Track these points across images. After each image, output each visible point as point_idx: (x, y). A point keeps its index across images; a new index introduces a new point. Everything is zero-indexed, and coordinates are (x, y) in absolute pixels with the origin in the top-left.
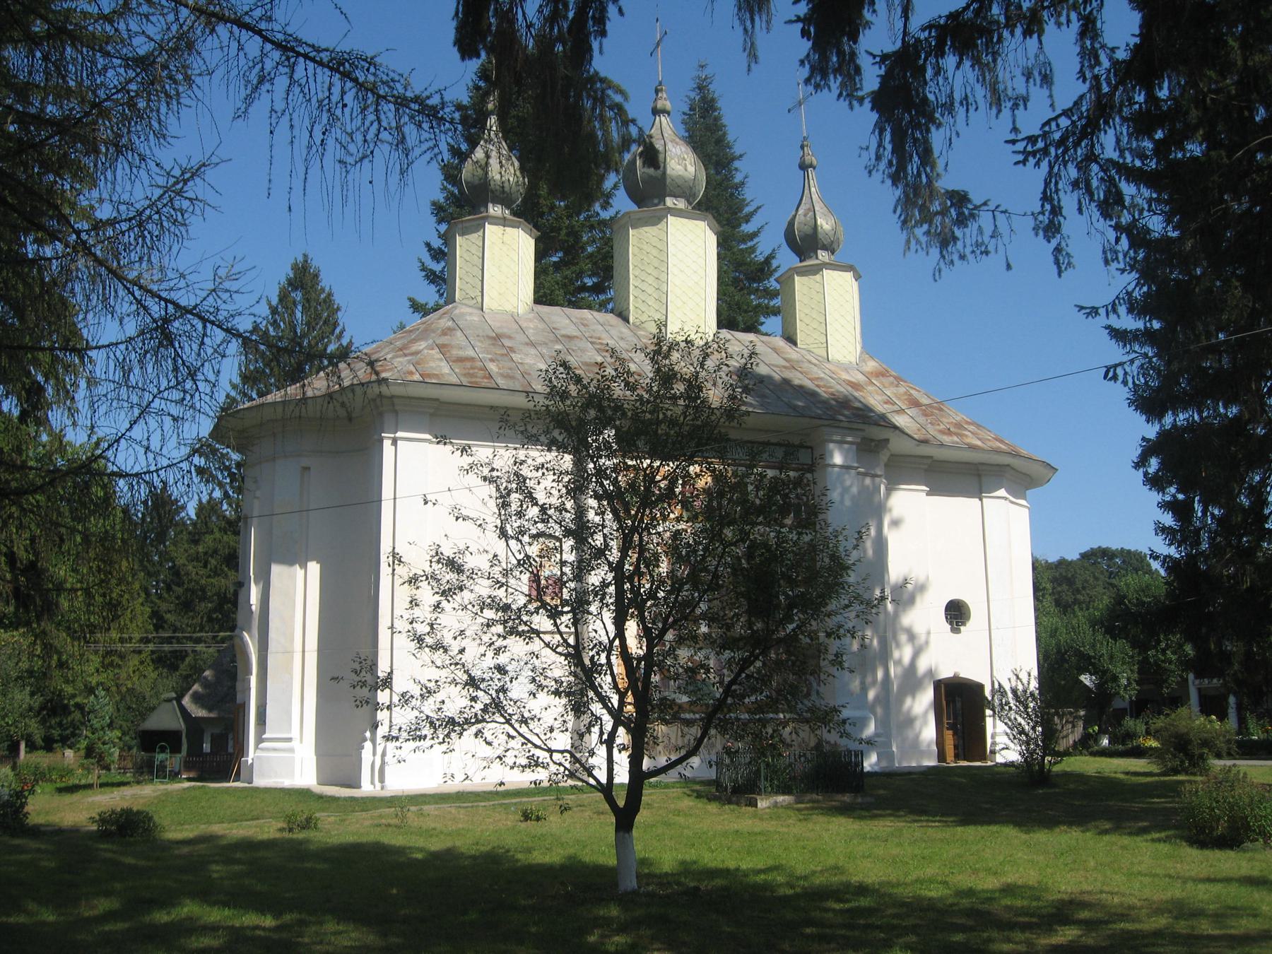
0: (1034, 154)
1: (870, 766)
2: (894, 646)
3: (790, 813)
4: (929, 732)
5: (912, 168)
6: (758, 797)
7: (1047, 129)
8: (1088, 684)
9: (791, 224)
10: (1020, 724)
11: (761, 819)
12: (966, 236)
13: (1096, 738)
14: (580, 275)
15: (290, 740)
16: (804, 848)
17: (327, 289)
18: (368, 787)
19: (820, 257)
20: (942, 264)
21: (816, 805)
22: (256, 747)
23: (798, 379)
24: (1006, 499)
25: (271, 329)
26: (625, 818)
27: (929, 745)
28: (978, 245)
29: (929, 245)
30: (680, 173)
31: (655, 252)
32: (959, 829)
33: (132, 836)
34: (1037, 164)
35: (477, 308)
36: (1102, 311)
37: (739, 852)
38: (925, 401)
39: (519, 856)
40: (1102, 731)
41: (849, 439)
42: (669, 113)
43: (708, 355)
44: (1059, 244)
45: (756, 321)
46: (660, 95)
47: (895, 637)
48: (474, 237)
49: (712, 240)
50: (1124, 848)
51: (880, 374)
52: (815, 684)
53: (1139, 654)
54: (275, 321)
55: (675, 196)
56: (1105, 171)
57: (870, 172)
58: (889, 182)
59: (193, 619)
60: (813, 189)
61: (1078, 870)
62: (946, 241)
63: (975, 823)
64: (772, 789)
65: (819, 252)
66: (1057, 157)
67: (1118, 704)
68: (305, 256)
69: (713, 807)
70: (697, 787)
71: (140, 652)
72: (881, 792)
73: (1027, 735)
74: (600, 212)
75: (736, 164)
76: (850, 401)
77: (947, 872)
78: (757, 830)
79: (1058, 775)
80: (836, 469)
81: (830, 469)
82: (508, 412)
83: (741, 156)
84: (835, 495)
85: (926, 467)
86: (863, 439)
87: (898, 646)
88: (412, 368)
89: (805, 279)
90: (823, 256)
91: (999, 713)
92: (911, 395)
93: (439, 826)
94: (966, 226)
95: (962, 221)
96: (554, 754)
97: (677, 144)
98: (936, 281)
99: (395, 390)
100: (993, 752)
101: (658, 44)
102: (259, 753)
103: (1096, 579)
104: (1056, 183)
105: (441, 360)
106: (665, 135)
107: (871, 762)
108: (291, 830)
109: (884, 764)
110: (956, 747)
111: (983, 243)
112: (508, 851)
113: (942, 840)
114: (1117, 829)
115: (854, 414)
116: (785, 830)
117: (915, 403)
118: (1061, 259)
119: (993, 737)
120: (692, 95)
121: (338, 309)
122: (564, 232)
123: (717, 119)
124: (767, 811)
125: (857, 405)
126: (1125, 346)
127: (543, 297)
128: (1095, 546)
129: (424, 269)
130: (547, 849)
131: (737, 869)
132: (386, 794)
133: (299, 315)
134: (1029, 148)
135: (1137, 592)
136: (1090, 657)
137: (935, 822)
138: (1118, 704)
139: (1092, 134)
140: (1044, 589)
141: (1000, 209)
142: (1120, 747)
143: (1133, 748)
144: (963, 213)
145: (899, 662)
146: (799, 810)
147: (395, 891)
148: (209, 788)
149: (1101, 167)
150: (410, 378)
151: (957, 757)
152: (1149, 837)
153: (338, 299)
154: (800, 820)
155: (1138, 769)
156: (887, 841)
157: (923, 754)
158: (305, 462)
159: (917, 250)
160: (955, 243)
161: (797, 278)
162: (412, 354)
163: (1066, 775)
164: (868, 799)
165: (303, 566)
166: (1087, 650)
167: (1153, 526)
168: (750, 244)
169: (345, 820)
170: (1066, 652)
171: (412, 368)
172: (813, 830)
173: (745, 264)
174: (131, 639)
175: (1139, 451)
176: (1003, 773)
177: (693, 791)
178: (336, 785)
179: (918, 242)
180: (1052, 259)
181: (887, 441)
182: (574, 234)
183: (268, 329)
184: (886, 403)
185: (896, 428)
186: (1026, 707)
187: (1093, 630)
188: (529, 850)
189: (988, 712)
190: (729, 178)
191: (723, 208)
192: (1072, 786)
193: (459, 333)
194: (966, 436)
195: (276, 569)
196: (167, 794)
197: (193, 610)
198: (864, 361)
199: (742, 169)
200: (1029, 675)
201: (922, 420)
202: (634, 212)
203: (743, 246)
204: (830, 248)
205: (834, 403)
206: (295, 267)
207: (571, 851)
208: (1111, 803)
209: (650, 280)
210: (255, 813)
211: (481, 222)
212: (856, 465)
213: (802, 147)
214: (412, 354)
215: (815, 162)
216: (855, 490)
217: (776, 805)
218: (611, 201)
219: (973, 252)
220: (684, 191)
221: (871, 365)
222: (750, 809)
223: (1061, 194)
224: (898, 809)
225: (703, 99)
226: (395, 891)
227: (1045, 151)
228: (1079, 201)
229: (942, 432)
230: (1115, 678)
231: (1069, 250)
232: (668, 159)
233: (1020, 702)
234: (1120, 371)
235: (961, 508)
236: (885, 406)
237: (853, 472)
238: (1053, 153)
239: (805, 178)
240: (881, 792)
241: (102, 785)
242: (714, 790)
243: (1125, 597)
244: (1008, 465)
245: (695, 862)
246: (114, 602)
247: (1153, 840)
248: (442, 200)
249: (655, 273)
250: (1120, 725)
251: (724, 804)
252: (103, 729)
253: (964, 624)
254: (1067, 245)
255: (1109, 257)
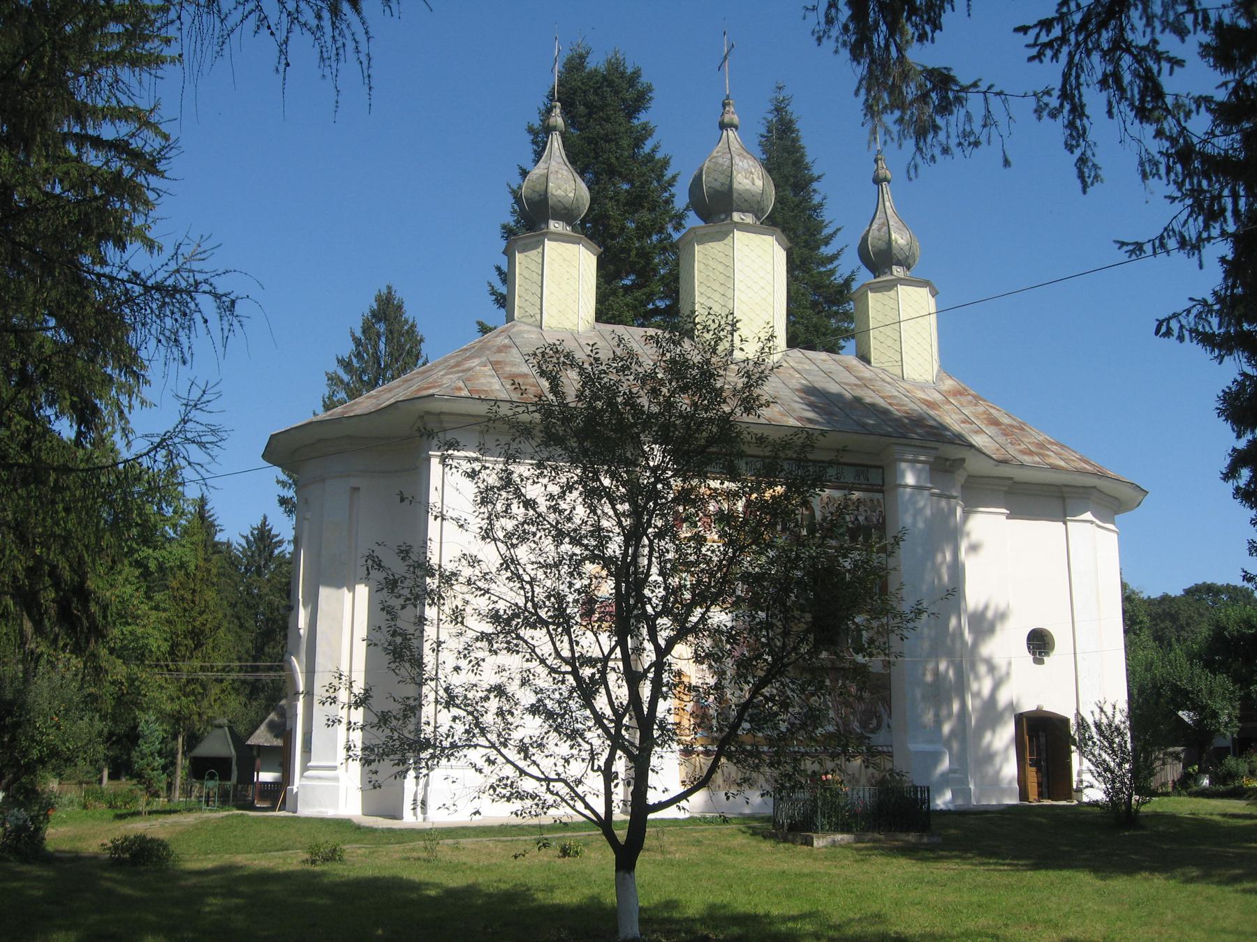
0: (1049, 44)
1: (945, 803)
2: (972, 677)
3: (848, 853)
4: (1010, 769)
5: (879, 39)
6: (814, 835)
7: (1065, 10)
8: (1187, 720)
9: (865, 239)
10: (1104, 761)
11: (815, 859)
12: (951, 125)
13: (1195, 778)
14: (650, 297)
15: (334, 768)
16: (851, 892)
17: (411, 321)
18: (409, 819)
19: (895, 273)
20: (918, 158)
21: (877, 845)
22: (302, 776)
23: (869, 397)
24: (1092, 522)
25: (354, 360)
26: (627, 855)
27: (1010, 782)
28: (966, 135)
29: (902, 135)
30: (747, 187)
31: (721, 268)
32: (1029, 873)
33: (144, 865)
34: (1055, 56)
35: (536, 326)
36: (1148, 248)
37: (777, 896)
38: (1006, 420)
39: (540, 896)
40: (1202, 771)
41: (922, 458)
42: (736, 128)
43: (721, 339)
44: (1083, 154)
45: (835, 345)
46: (727, 109)
47: (973, 666)
48: (534, 254)
49: (781, 256)
50: (1209, 899)
51: (958, 393)
52: (885, 717)
53: (1241, 689)
54: (359, 353)
55: (743, 211)
56: (1139, 62)
57: (819, 39)
58: (845, 54)
59: (274, 648)
60: (887, 204)
61: (1151, 924)
62: (923, 131)
63: (1047, 867)
64: (830, 826)
65: (894, 267)
66: (1078, 44)
67: (1218, 742)
68: (389, 288)
69: (767, 846)
70: (756, 824)
71: (221, 681)
72: (953, 831)
73: (1112, 772)
74: (673, 233)
75: (815, 185)
76: (924, 419)
77: (1000, 923)
78: (806, 871)
79: (1147, 816)
80: (908, 490)
81: (901, 489)
82: (498, 403)
83: (819, 177)
84: (907, 519)
85: (1006, 488)
86: (937, 458)
87: (977, 678)
88: (461, 384)
89: (879, 295)
90: (898, 271)
91: (1082, 745)
92: (991, 414)
93: (469, 860)
94: (951, 113)
95: (945, 108)
96: (552, 784)
97: (744, 157)
98: (910, 179)
99: (446, 407)
100: (1079, 790)
101: (725, 58)
102: (305, 782)
103: (1201, 615)
104: (1078, 77)
105: (493, 376)
106: (733, 149)
107: (943, 800)
108: (313, 862)
109: (960, 802)
110: (1040, 785)
111: (972, 132)
112: (528, 889)
113: (1006, 886)
114: (1205, 877)
115: (927, 432)
116: (836, 871)
117: (995, 422)
118: (1086, 173)
119: (1079, 774)
120: (770, 117)
121: (422, 340)
122: (634, 253)
123: (795, 140)
124: (824, 850)
125: (933, 423)
126: (1213, 350)
127: (602, 315)
128: (1200, 582)
129: (493, 292)
130: (572, 888)
131: (767, 915)
132: (427, 825)
133: (382, 346)
134: (1044, 38)
135: (1238, 624)
136: (1187, 692)
137: (1003, 865)
138: (1218, 742)
139: (1121, 12)
140: (1141, 622)
141: (994, 90)
142: (1222, 788)
143: (1235, 789)
144: (947, 98)
145: (977, 695)
146: (858, 850)
147: (380, 932)
148: (248, 816)
149: (1134, 57)
150: (458, 394)
151: (1041, 795)
152: (1239, 887)
153: (421, 330)
154: (856, 861)
155: (1237, 811)
156: (945, 886)
157: (1004, 792)
158: (355, 482)
159: (885, 142)
160: (936, 133)
161: (870, 294)
162: (463, 371)
163: (1157, 817)
164: (936, 840)
165: (352, 589)
166: (1184, 684)
167: (1247, 546)
168: (830, 267)
169: (374, 852)
170: (1162, 686)
171: (461, 384)
172: (867, 872)
173: (824, 287)
174: (212, 667)
175: (1228, 461)
176: (1088, 813)
177: (749, 828)
178: (380, 816)
179: (887, 132)
180: (1075, 171)
181: (963, 460)
182: (645, 255)
183: (351, 360)
184: (963, 422)
185: (971, 446)
186: (1111, 743)
187: (1191, 664)
188: (551, 889)
189: (1073, 748)
190: (807, 199)
191: (801, 230)
192: (1161, 828)
193: (515, 351)
194: (1048, 456)
195: (325, 593)
196: (207, 821)
197: (274, 640)
198: (941, 380)
199: (820, 191)
200: (1114, 708)
201: (1001, 439)
202: (701, 227)
203: (823, 269)
204: (906, 263)
205: (906, 421)
206: (379, 299)
207: (596, 890)
208: (1203, 847)
209: (717, 297)
210: (286, 843)
211: (541, 238)
212: (929, 485)
213: (876, 161)
214: (463, 371)
215: (889, 176)
216: (928, 512)
217: (834, 843)
218: (683, 222)
219: (960, 144)
220: (751, 205)
221: (949, 384)
222: (806, 848)
223: (1083, 89)
224: (966, 851)
225: (781, 120)
226: (380, 932)
227: (1063, 40)
228: (1110, 104)
229: (1023, 452)
230: (1215, 715)
231: (1096, 160)
232: (735, 173)
233: (1105, 737)
234: (1174, 325)
235: (1045, 532)
236: (963, 425)
237: (926, 492)
238: (1073, 40)
239: (880, 193)
240: (953, 831)
241: (150, 813)
242: (771, 827)
243: (1225, 629)
244: (1094, 487)
245: (724, 907)
246: (197, 630)
247: (1244, 891)
248: (512, 224)
249: (721, 290)
250: (1222, 764)
251: (779, 843)
252: (152, 754)
253: (1047, 654)
254: (1094, 155)
255: (1148, 169)
